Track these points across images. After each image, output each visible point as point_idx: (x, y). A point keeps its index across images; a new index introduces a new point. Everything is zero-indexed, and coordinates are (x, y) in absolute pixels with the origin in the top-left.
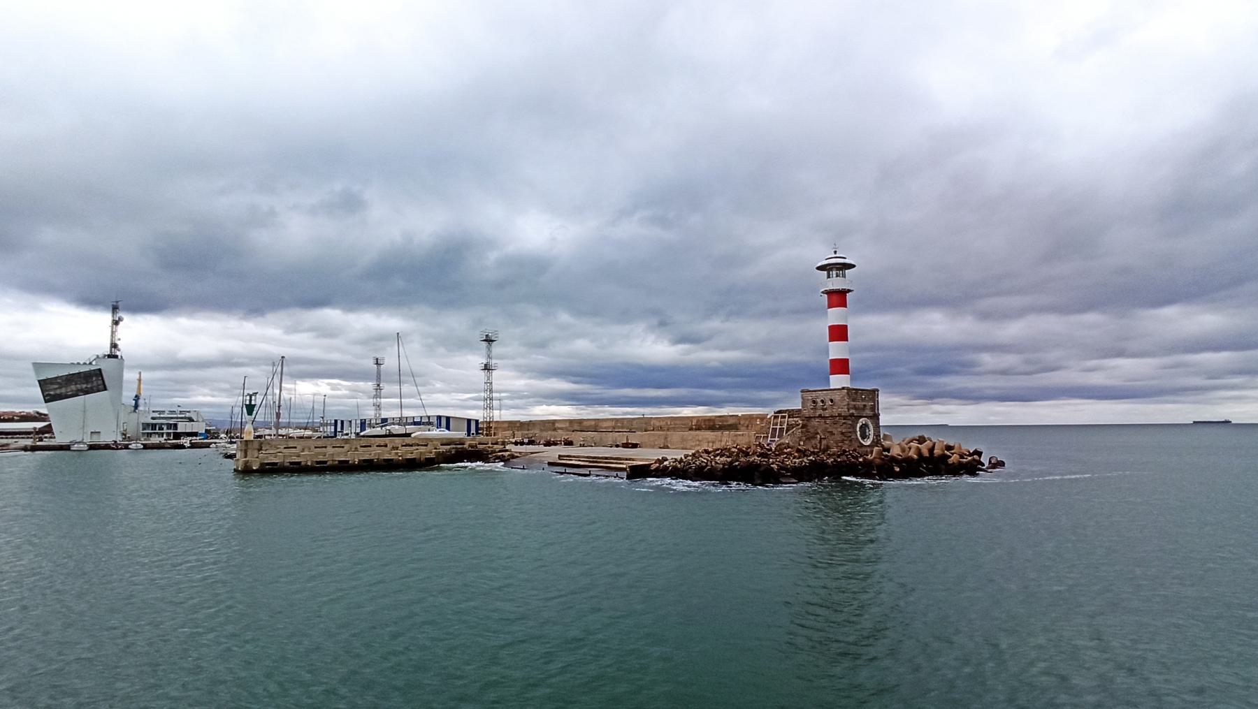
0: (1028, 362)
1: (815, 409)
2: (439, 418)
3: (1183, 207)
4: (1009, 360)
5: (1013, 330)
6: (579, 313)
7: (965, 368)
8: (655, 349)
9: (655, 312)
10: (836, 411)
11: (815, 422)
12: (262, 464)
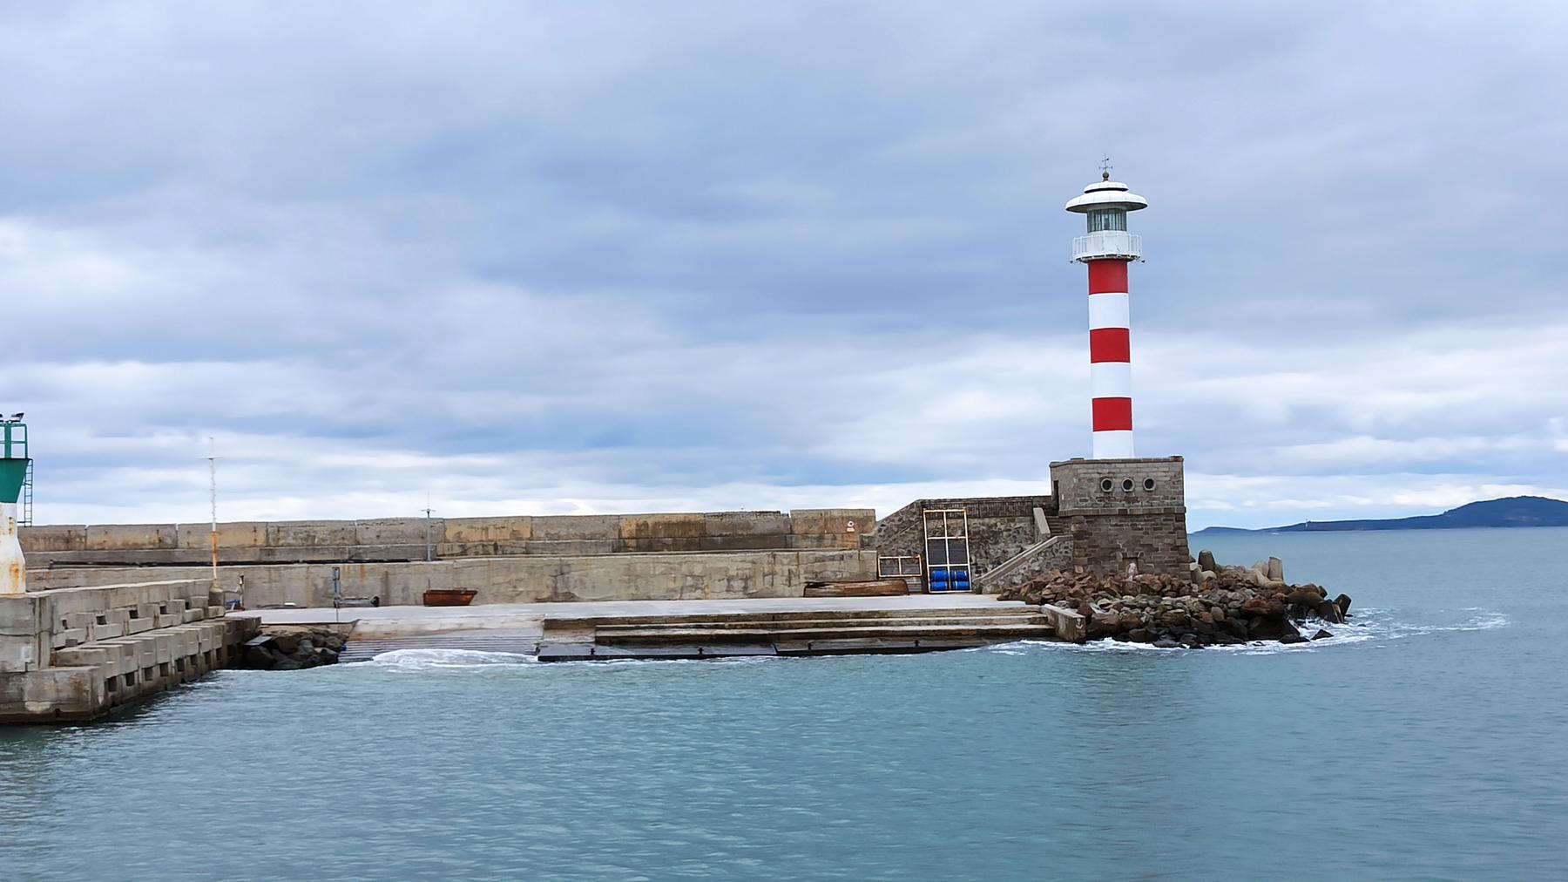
11: (1107, 527)
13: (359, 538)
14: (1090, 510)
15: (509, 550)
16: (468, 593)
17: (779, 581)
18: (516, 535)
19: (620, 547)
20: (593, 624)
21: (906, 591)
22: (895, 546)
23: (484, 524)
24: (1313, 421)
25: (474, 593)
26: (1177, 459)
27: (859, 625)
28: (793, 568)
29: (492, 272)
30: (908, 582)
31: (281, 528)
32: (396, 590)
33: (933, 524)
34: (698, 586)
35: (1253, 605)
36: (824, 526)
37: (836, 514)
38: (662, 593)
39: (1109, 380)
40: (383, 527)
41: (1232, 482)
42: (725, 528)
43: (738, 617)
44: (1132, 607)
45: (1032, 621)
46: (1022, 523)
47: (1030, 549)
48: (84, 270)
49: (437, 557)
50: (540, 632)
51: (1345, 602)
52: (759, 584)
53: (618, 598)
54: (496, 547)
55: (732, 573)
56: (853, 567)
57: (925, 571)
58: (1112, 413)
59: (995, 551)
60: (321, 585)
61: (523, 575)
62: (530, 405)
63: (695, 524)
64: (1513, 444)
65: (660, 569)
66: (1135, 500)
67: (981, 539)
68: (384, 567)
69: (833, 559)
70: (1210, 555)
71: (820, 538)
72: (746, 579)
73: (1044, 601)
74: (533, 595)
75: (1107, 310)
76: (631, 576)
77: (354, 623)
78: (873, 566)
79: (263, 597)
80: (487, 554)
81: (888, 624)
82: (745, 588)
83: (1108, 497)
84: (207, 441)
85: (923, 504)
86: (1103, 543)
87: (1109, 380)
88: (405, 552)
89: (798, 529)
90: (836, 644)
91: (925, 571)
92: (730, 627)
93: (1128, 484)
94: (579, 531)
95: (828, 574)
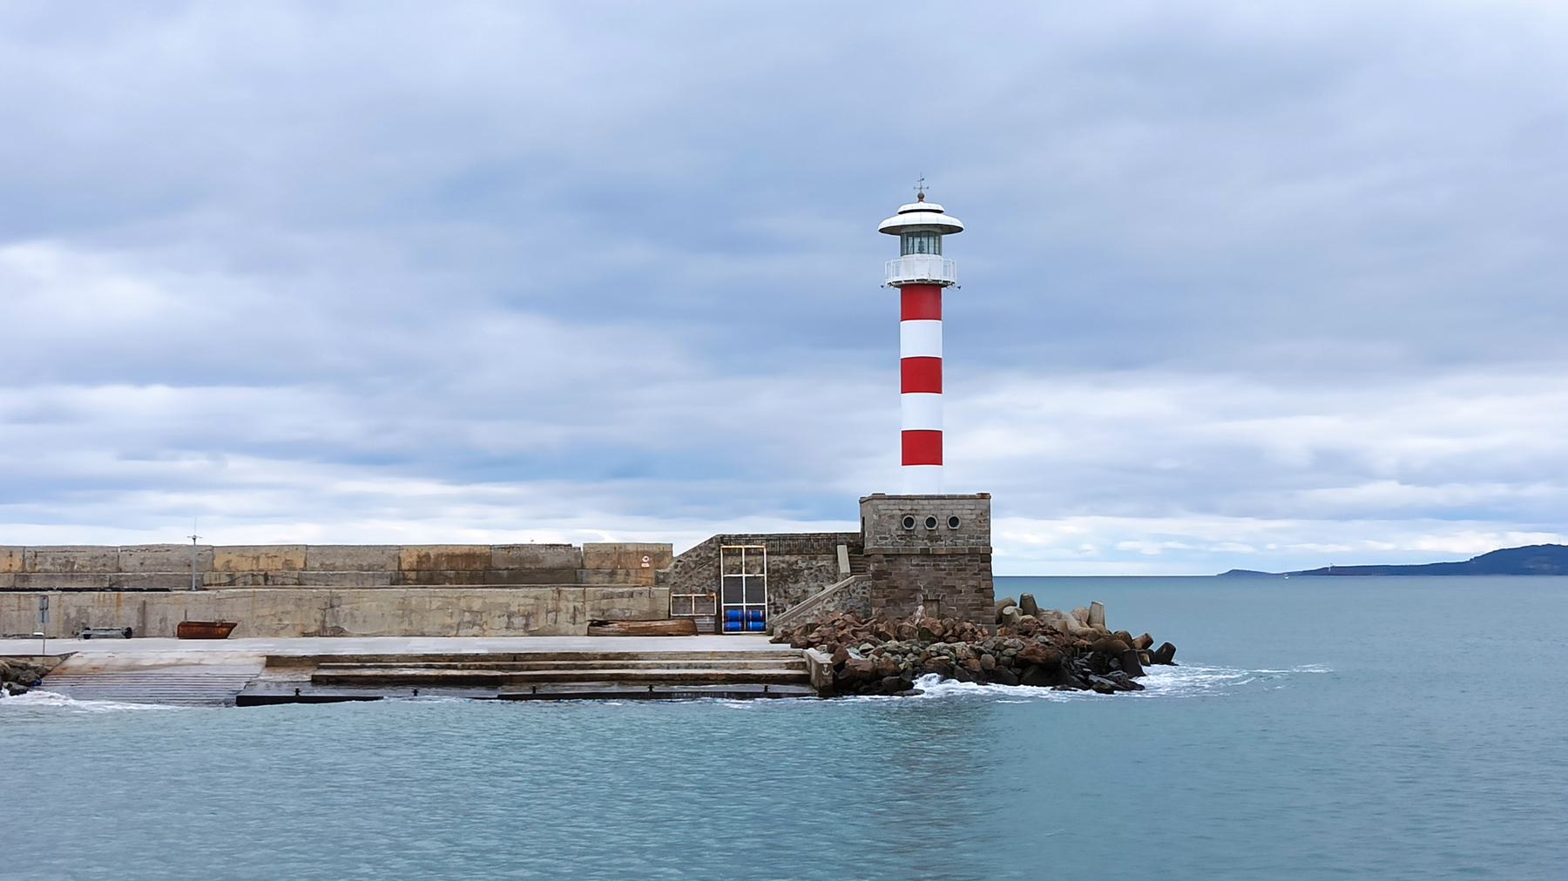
11: (906, 566)
13: (121, 565)
14: (890, 549)
15: (281, 580)
16: (223, 625)
17: (563, 617)
18: (288, 564)
19: (399, 579)
20: (317, 661)
21: (692, 630)
22: (689, 583)
23: (255, 552)
24: (1335, 465)
25: (232, 626)
26: (984, 496)
27: (603, 667)
28: (579, 605)
29: (520, 302)
30: (697, 621)
31: (38, 553)
32: (153, 622)
33: (731, 561)
34: (476, 623)
35: (1028, 653)
36: (615, 562)
37: (631, 549)
38: (437, 628)
39: (918, 411)
40: (148, 554)
41: (1252, 525)
42: (512, 561)
43: (477, 657)
44: (894, 653)
45: (790, 666)
46: (824, 562)
47: (829, 588)
48: (109, 292)
49: (203, 587)
50: (258, 670)
52: (542, 621)
53: (391, 634)
54: (266, 577)
55: (514, 609)
56: (643, 605)
57: (719, 610)
58: (922, 447)
59: (795, 589)
60: (73, 614)
61: (290, 607)
62: (551, 435)
63: (480, 556)
64: (1539, 491)
65: (436, 603)
66: (938, 539)
67: (780, 578)
68: (141, 596)
69: (621, 595)
70: (1031, 598)
71: (613, 574)
72: (527, 616)
73: (810, 645)
74: (299, 628)
75: (919, 338)
76: (405, 610)
77: (66, 657)
78: (664, 605)
79: (11, 626)
80: (256, 584)
81: (634, 666)
82: (527, 625)
83: (910, 535)
84: (237, 465)
85: (722, 539)
86: (903, 583)
87: (918, 411)
88: (169, 581)
89: (589, 564)
91: (719, 610)
92: (464, 668)
93: (931, 522)
94: (356, 562)
95: (616, 612)
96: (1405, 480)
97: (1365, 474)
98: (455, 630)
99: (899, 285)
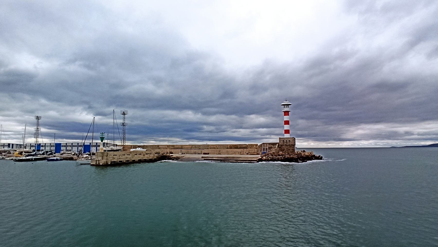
0: (217, 129)
1: (284, 143)
2: (9, 144)
3: (255, 88)
4: (212, 128)
5: (213, 119)
6: (49, 99)
7: (200, 130)
8: (86, 117)
9: (83, 102)
10: (291, 144)
11: (284, 147)
12: (112, 162)
34: (235, 153)
51: (322, 157)
56: (254, 151)
58: (287, 132)
62: (306, 132)
67: (270, 148)
83: (284, 143)
84: (272, 136)
90: (231, 161)
96: (418, 135)
97: (413, 134)
98: (232, 154)
99: (284, 112)
